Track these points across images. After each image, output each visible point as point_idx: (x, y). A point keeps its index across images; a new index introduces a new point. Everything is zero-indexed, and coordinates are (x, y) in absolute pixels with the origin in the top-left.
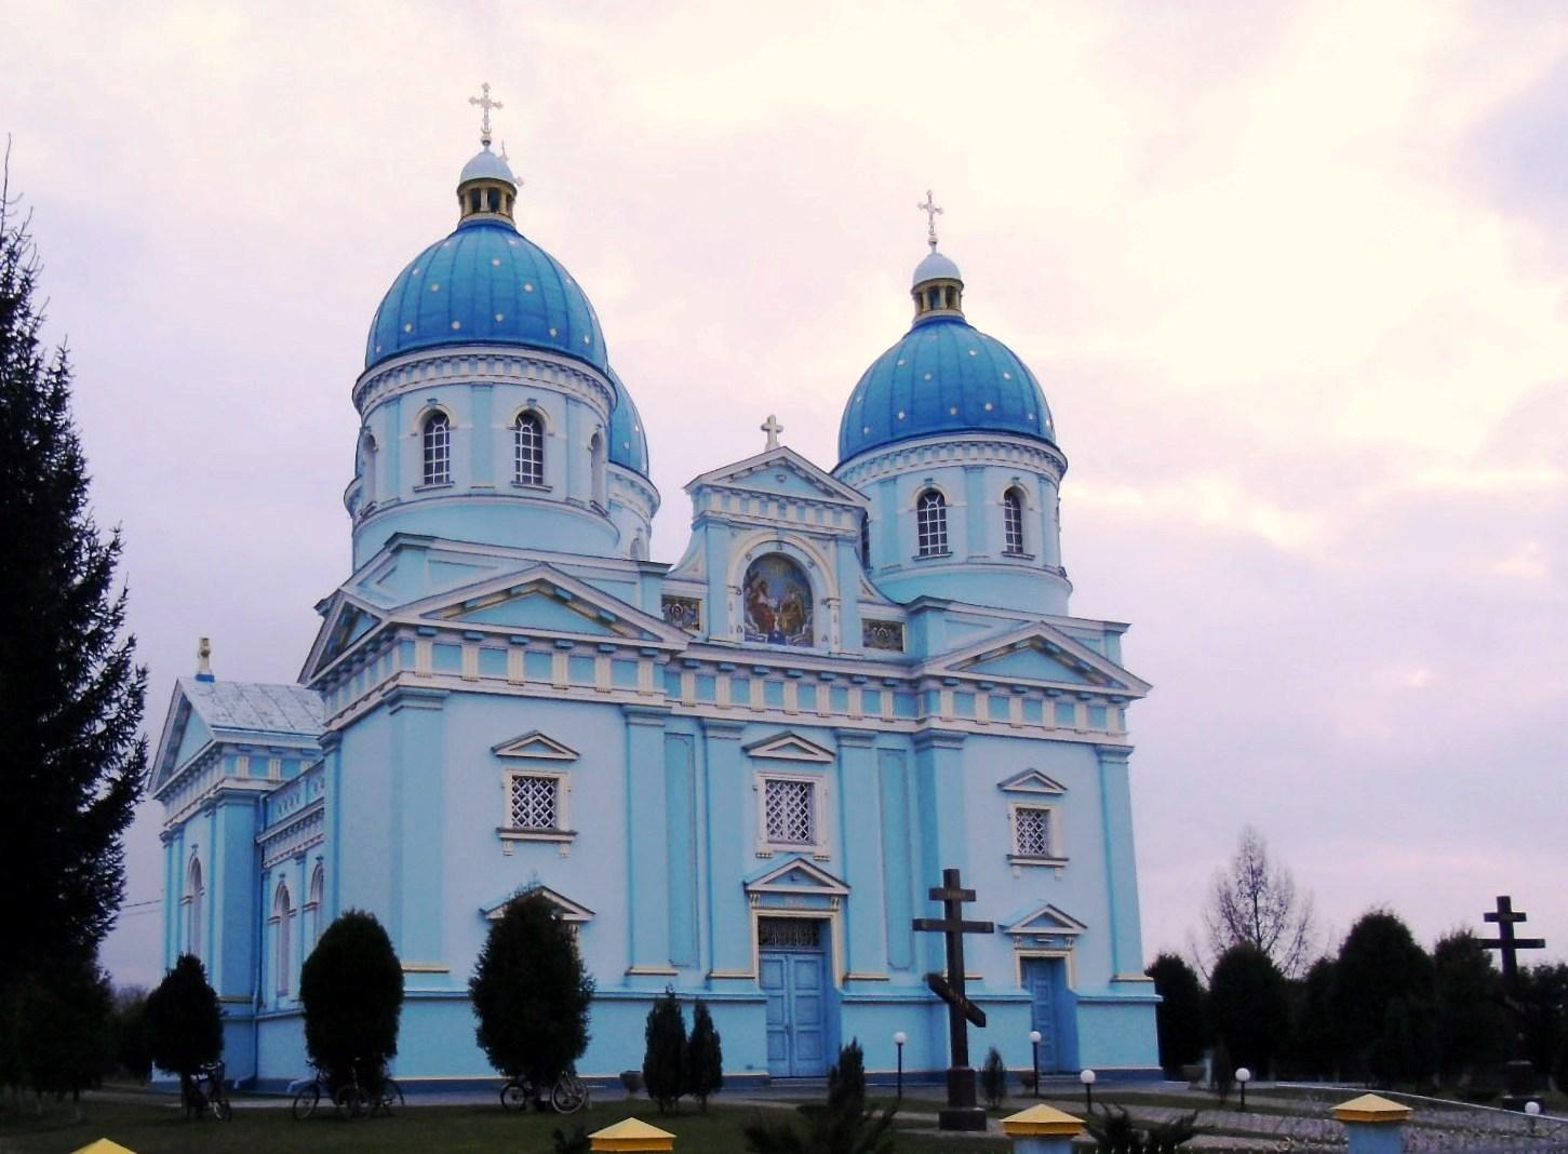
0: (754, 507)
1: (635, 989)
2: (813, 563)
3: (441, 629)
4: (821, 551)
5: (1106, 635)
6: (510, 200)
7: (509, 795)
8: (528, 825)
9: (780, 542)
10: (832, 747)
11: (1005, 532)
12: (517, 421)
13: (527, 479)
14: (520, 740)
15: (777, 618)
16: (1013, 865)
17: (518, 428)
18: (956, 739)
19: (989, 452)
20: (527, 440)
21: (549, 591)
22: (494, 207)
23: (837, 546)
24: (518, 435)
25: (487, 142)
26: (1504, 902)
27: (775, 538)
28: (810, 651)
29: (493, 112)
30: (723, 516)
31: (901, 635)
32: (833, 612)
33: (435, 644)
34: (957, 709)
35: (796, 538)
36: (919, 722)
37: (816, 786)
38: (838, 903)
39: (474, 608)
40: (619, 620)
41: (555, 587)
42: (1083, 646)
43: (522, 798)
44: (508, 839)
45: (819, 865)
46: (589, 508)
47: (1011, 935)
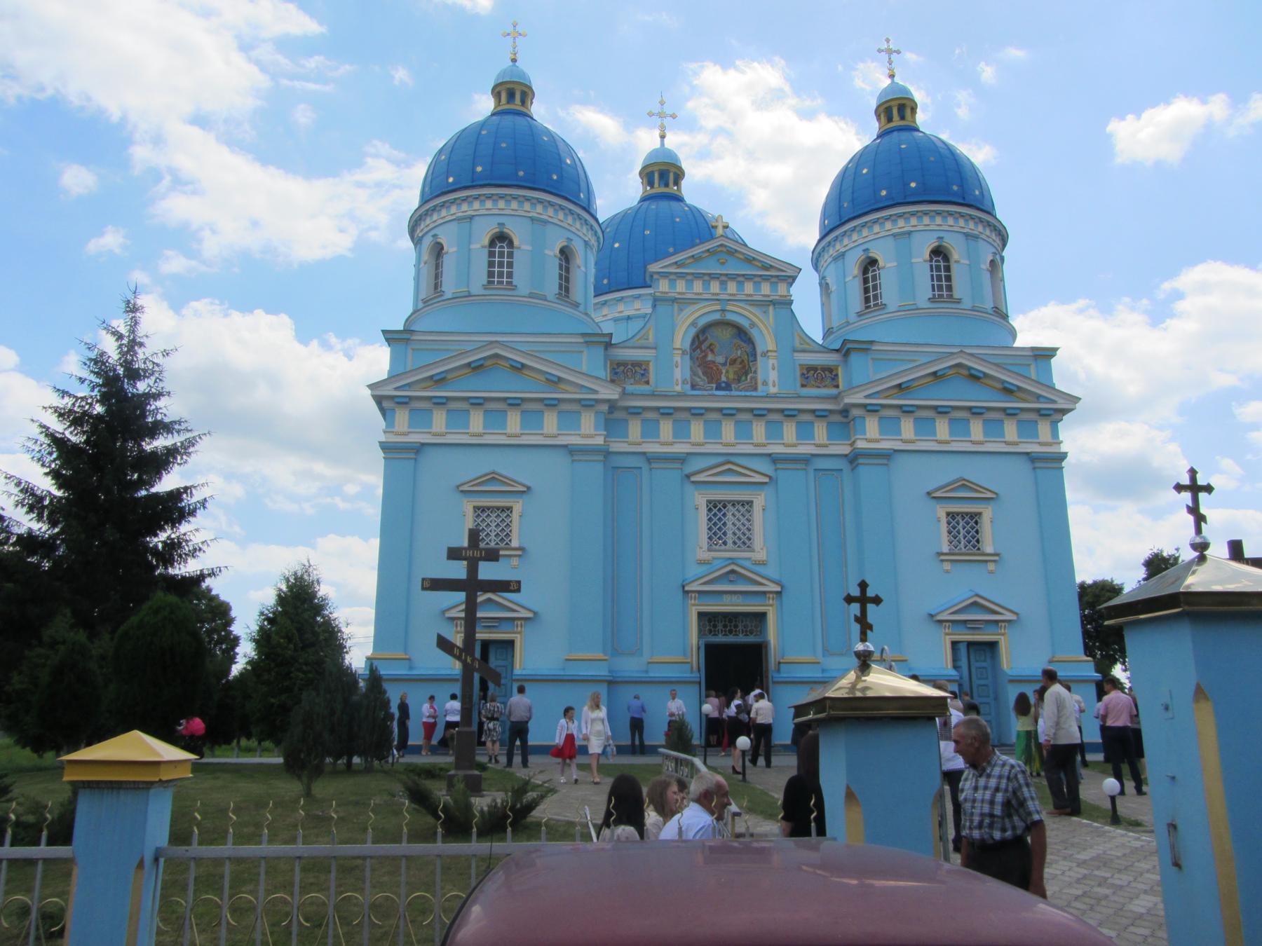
0: (698, 286)
1: (651, 675)
2: (753, 325)
3: (883, 406)
4: (761, 316)
5: (1036, 360)
7: (944, 527)
8: (961, 549)
9: (723, 311)
10: (770, 471)
11: (930, 283)
12: (930, 255)
13: (941, 296)
14: (471, 481)
15: (724, 371)
16: (942, 561)
17: (931, 261)
19: (914, 221)
20: (938, 268)
21: (965, 372)
22: (902, 118)
23: (775, 308)
24: (931, 266)
25: (514, 60)
27: (718, 307)
28: (754, 394)
29: (519, 40)
30: (670, 294)
31: (837, 375)
32: (771, 362)
33: (559, 412)
34: (882, 430)
35: (734, 305)
38: (773, 599)
39: (908, 388)
40: (1019, 388)
41: (969, 368)
42: (1009, 370)
43: (954, 529)
44: (947, 560)
45: (757, 568)
46: (992, 313)
47: (940, 622)
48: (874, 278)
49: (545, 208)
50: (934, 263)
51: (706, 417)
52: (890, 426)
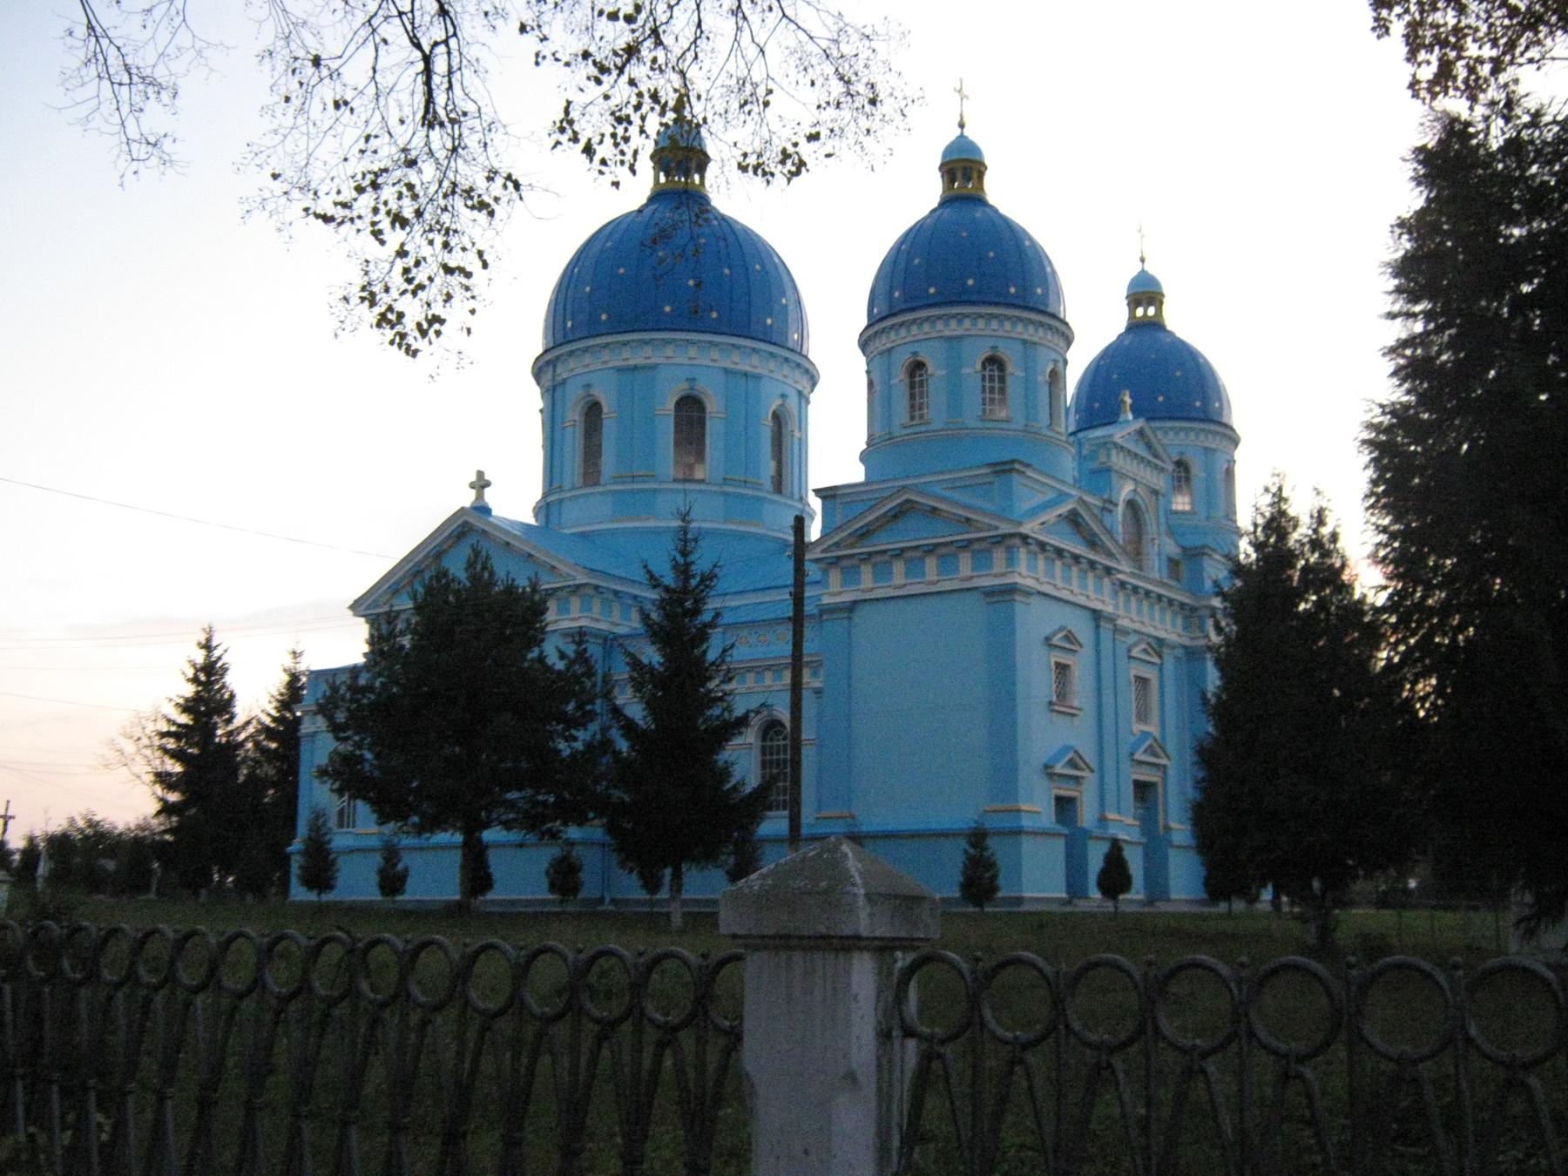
6: (981, 175)
18: (1028, 593)
20: (992, 379)
25: (962, 126)
26: (480, 474)
34: (876, 578)
36: (1192, 639)
37: (1073, 667)
48: (921, 384)
49: (1026, 327)
50: (987, 373)
51: (873, 560)
52: (851, 574)
